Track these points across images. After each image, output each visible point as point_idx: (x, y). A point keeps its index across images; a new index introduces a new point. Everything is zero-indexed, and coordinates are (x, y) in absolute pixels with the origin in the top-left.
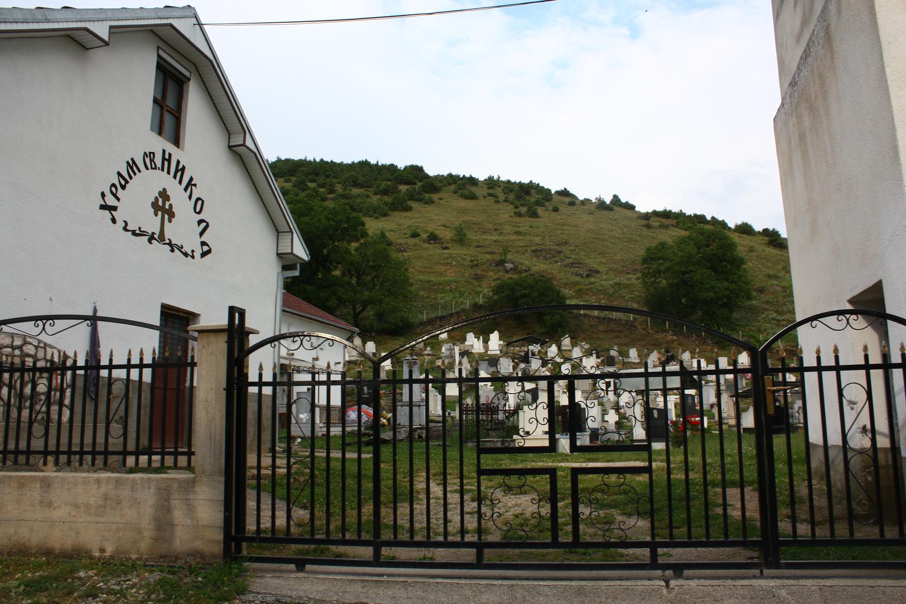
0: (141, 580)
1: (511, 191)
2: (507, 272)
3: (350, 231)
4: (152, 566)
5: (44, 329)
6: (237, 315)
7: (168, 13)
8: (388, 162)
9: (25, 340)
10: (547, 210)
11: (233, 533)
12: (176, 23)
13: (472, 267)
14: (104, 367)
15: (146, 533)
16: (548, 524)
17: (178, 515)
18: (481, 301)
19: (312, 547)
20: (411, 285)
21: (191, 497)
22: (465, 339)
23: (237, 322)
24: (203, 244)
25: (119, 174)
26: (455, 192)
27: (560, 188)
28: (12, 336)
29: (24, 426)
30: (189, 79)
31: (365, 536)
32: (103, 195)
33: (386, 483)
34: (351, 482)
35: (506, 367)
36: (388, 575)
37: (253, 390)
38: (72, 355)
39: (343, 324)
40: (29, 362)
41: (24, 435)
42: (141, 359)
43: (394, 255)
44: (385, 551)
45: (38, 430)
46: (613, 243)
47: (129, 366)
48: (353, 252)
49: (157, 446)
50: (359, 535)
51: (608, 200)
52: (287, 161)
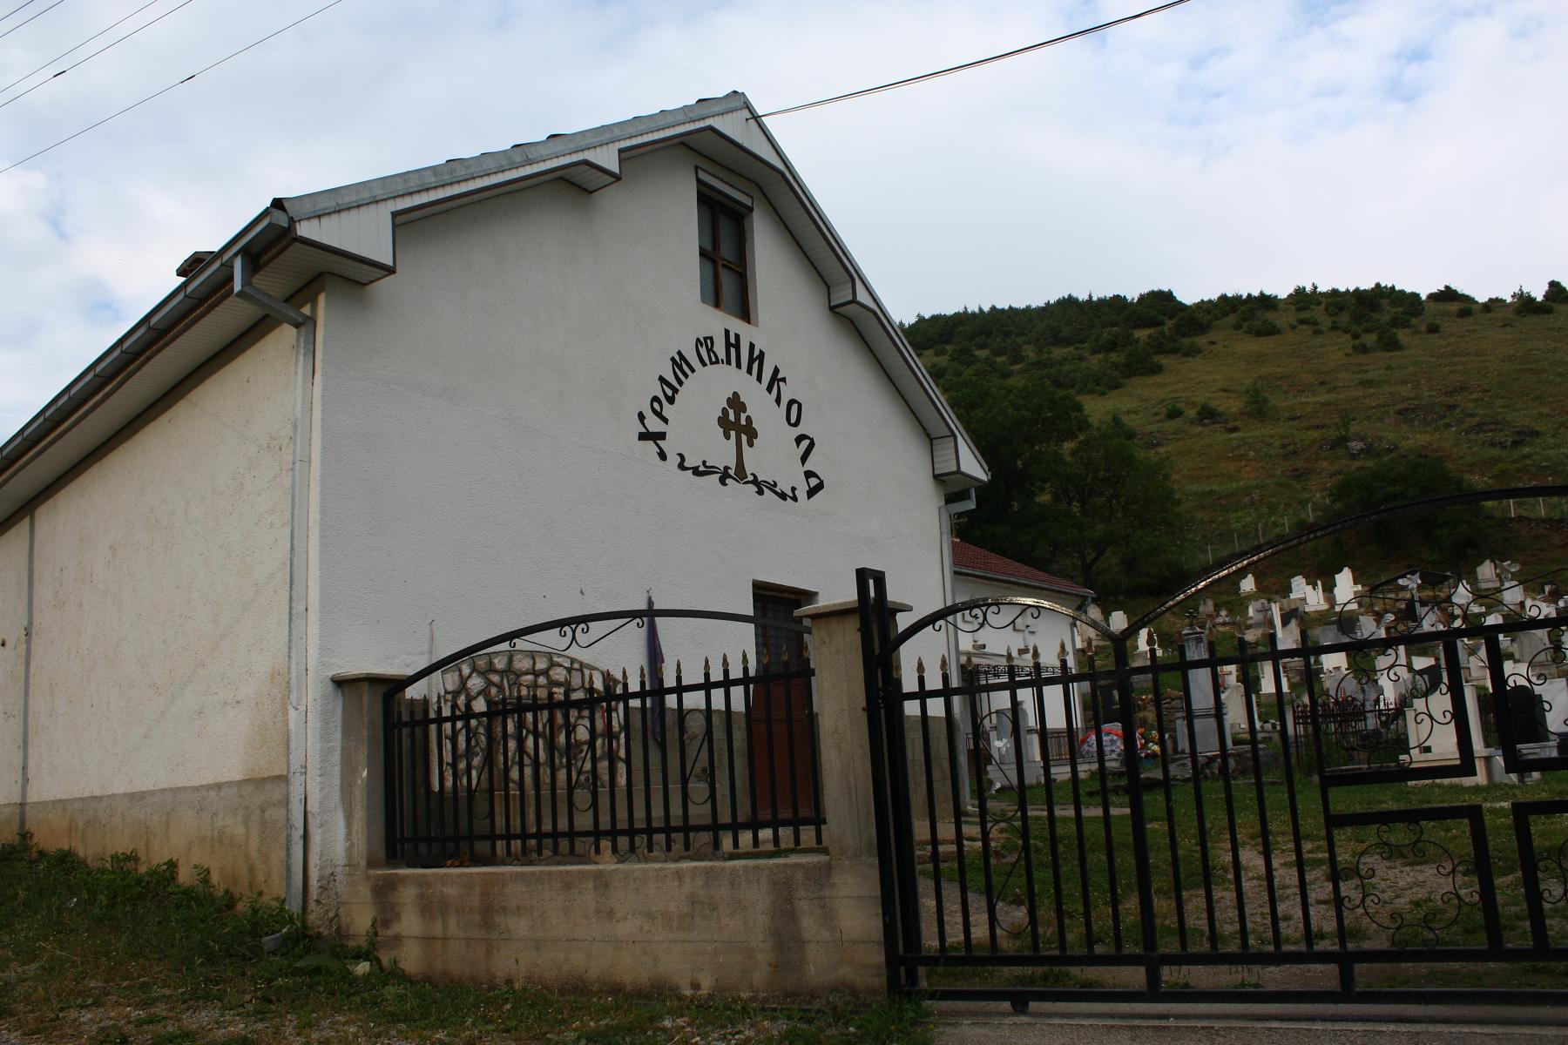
0: (758, 1032)
1: (1341, 309)
2: (1353, 457)
3: (1064, 421)
4: (775, 1010)
5: (574, 638)
6: (871, 582)
7: (703, 111)
8: (1109, 294)
9: (551, 660)
10: (1416, 332)
11: (901, 951)
12: (719, 123)
13: (1285, 457)
14: (670, 691)
15: (760, 957)
16: (1479, 918)
17: (809, 924)
18: (1310, 516)
19: (1040, 970)
20: (1179, 503)
21: (827, 893)
22: (1288, 589)
23: (872, 594)
24: (809, 474)
25: (662, 379)
26: (1237, 327)
27: (1437, 286)
28: (532, 655)
29: (561, 792)
30: (751, 209)
31: (1130, 948)
32: (641, 417)
33: (1158, 858)
34: (1097, 858)
35: (1369, 628)
36: (1178, 1017)
37: (912, 708)
38: (619, 677)
39: (1063, 585)
40: (559, 693)
41: (563, 808)
42: (726, 672)
43: (1141, 454)
44: (1168, 974)
45: (582, 797)
46: (1561, 375)
47: (707, 686)
48: (1069, 459)
49: (766, 815)
50: (1119, 947)
51: (1539, 294)
52: (935, 318)
